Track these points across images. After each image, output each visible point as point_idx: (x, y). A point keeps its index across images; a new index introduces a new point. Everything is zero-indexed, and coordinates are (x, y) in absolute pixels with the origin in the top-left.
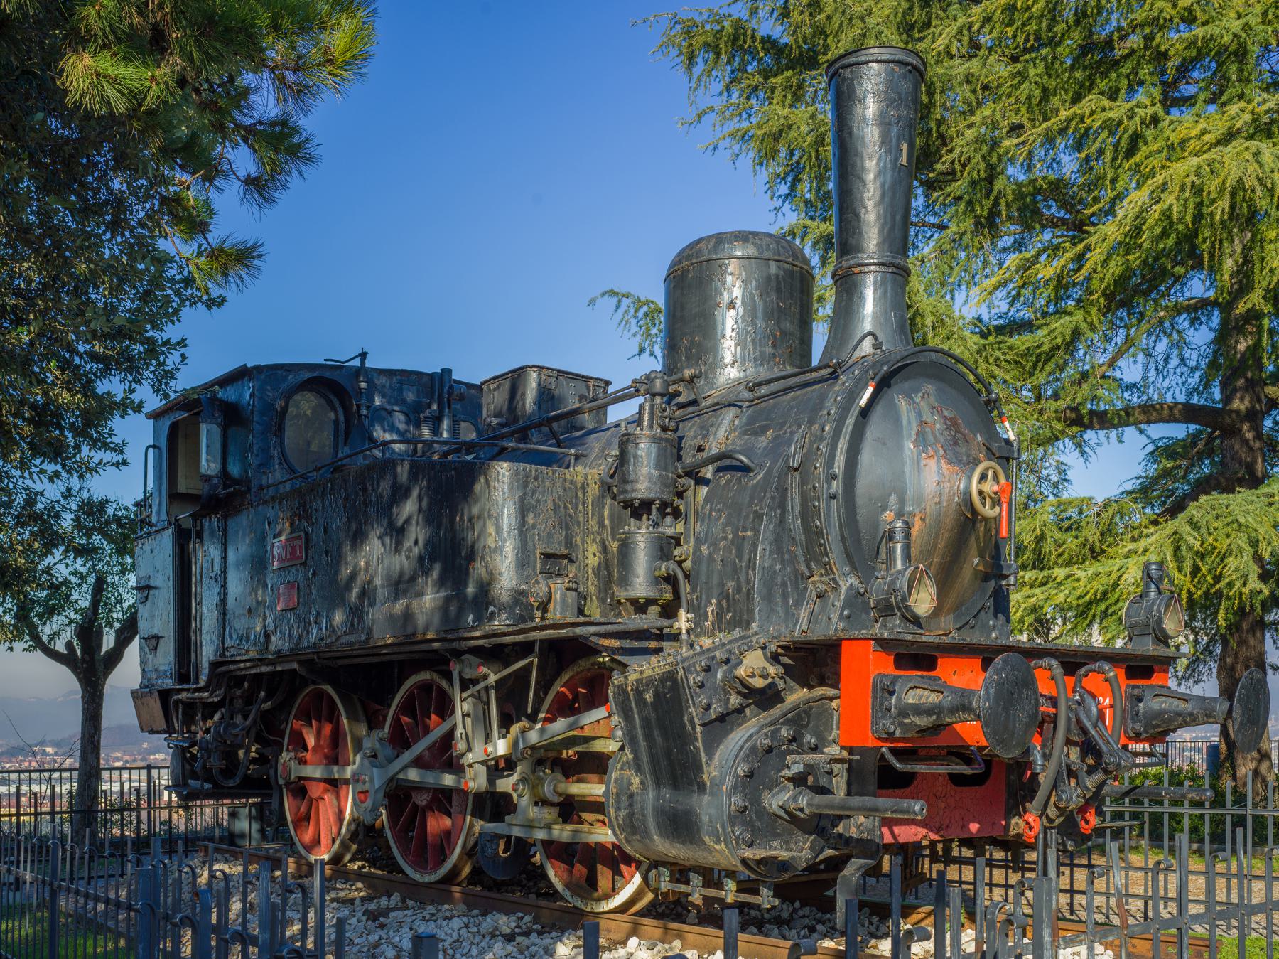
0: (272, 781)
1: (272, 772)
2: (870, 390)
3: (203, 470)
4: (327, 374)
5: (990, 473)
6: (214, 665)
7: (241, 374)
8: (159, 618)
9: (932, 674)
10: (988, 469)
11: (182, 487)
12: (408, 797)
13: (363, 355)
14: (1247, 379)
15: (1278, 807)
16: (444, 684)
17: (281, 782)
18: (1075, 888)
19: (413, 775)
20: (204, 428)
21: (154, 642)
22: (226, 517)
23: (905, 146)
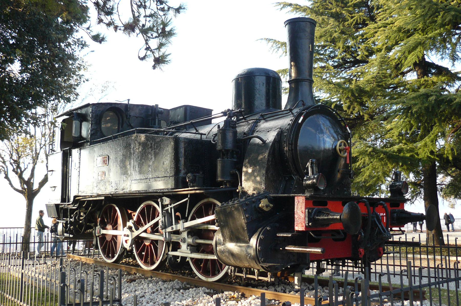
0: (94, 234)
1: (94, 232)
2: (302, 118)
3: (73, 135)
4: (117, 106)
5: (343, 143)
6: (75, 197)
7: (88, 105)
8: (56, 179)
9: (326, 207)
10: (342, 142)
11: (65, 140)
12: (142, 242)
13: (129, 100)
14: (296, 285)
15: (460, 240)
16: (156, 205)
17: (97, 235)
18: (393, 267)
19: (144, 235)
20: (74, 122)
21: (54, 189)
22: (80, 150)
23: (310, 45)
